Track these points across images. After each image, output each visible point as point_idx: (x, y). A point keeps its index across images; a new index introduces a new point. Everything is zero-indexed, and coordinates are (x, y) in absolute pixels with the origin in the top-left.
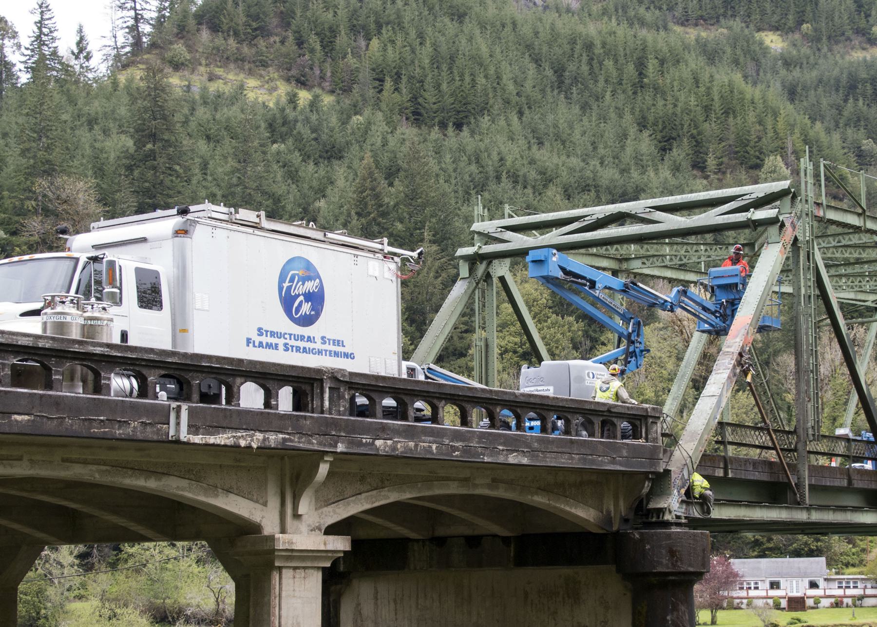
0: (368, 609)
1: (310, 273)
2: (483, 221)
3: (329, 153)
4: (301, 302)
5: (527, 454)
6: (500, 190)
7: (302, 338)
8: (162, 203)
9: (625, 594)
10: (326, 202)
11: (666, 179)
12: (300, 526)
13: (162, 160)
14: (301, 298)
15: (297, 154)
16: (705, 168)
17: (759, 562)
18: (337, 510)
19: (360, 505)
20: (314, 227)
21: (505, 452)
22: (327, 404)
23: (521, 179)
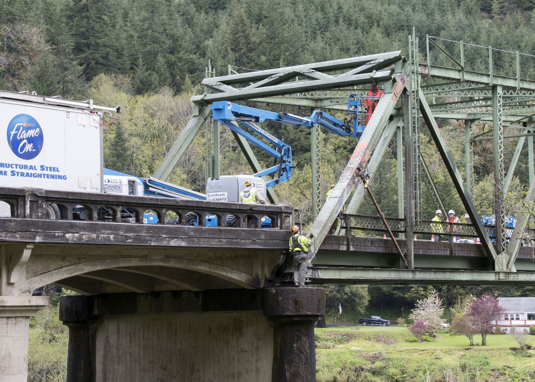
0: (113, 340)
1: (33, 124)
2: (212, 77)
3: (216, 5)
4: (25, 143)
5: (185, 240)
6: (338, 30)
7: (26, 167)
8: (93, 43)
9: (270, 330)
10: (213, 41)
11: (460, 20)
12: (13, 290)
13: (93, 12)
14: (25, 141)
15: (192, 5)
16: (491, 10)
17: (520, 300)
18: (43, 279)
19: (61, 275)
20: (36, 94)
21: (167, 239)
22: (28, 211)
23: (353, 22)
